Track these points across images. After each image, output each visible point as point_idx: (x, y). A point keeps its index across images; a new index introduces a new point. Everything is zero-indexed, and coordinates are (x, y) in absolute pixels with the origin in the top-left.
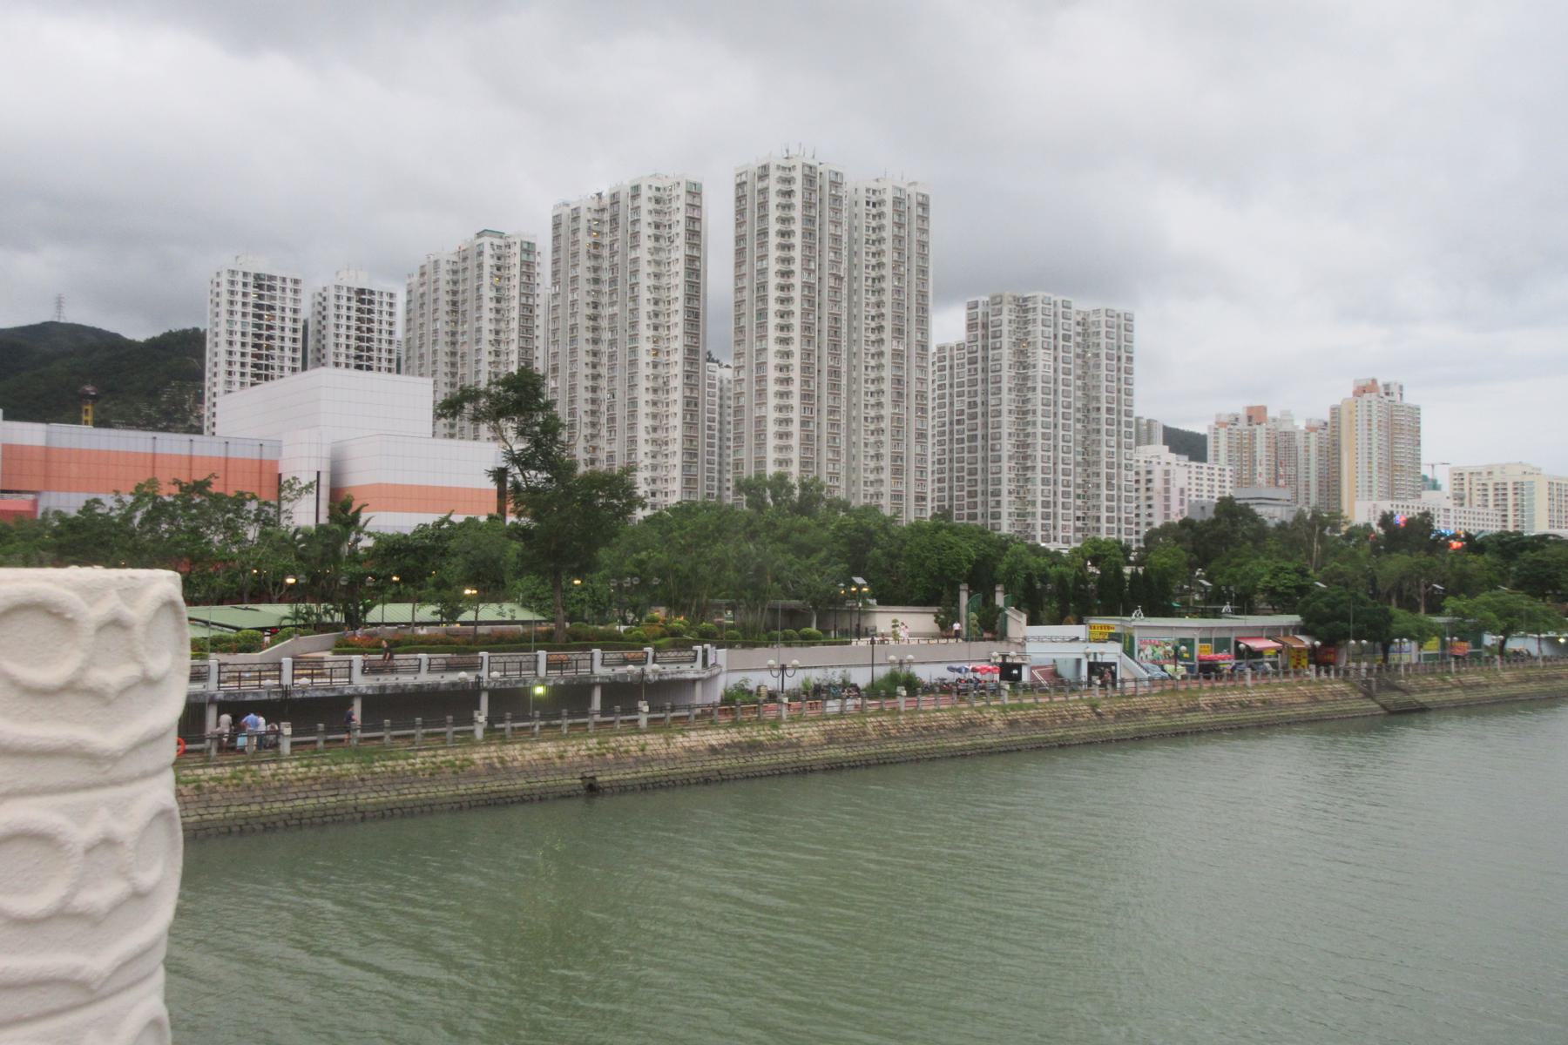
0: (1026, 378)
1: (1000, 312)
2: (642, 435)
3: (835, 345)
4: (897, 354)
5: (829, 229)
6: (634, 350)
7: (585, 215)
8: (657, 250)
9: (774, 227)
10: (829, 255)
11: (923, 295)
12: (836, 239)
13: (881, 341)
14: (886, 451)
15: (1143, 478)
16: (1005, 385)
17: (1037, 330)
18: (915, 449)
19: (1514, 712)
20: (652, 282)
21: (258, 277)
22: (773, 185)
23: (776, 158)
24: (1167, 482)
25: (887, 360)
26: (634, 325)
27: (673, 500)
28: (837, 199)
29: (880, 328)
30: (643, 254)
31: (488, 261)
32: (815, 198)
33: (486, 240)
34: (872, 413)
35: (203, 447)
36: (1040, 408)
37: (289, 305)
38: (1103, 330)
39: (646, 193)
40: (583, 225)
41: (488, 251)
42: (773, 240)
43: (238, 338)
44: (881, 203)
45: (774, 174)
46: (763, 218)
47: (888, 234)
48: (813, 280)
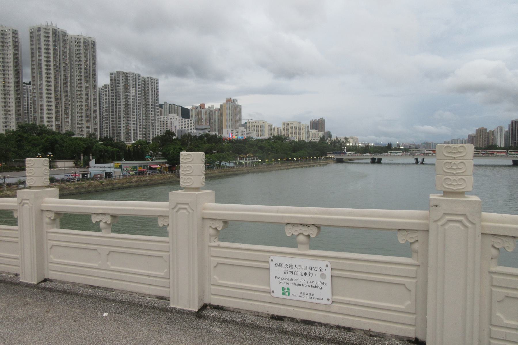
0: (128, 95)
1: (119, 77)
4: (86, 87)
10: (62, 57)
15: (165, 123)
16: (121, 97)
18: (93, 115)
24: (171, 124)
25: (83, 89)
28: (64, 40)
32: (57, 39)
34: (79, 104)
36: (132, 104)
45: (42, 31)
48: (58, 64)
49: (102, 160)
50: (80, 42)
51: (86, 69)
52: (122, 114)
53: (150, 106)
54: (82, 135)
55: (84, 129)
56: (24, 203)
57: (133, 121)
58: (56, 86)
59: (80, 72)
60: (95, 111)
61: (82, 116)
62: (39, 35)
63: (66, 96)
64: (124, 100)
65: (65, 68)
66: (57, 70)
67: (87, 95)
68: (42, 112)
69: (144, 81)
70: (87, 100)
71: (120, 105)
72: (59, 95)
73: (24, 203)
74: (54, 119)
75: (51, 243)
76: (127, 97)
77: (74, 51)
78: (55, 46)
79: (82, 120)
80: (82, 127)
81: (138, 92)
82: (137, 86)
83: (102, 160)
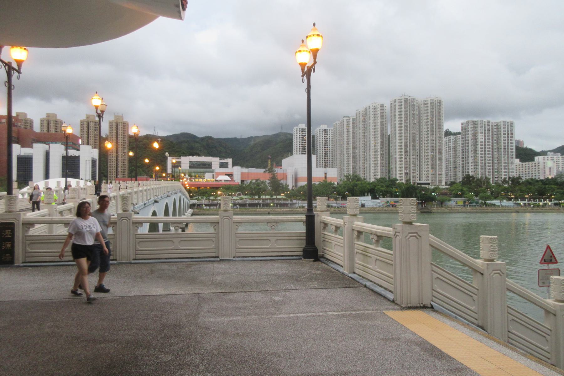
0: (476, 142)
2: (372, 162)
3: (414, 140)
4: (432, 140)
6: (370, 144)
7: (361, 113)
9: (397, 113)
10: (412, 118)
12: (414, 114)
13: (428, 137)
14: (430, 163)
15: (537, 165)
16: (470, 144)
17: (479, 129)
18: (438, 162)
20: (373, 127)
22: (397, 104)
23: (397, 98)
24: (544, 166)
25: (429, 142)
26: (370, 138)
27: (379, 177)
28: (414, 105)
29: (428, 134)
30: (371, 121)
31: (345, 123)
33: (345, 118)
34: (426, 154)
35: (205, 180)
36: (480, 150)
38: (502, 127)
39: (371, 107)
40: (361, 115)
41: (345, 121)
42: (397, 116)
43: (298, 143)
44: (428, 103)
45: (397, 101)
46: (395, 111)
47: (429, 111)
49: (21, 173)
50: (428, 103)
51: (432, 125)
52: (471, 160)
53: (503, 150)
54: (428, 180)
55: (430, 175)
56: (397, 236)
58: (406, 143)
59: (428, 128)
60: (440, 159)
61: (428, 165)
62: (395, 105)
63: (414, 149)
65: (414, 127)
66: (407, 130)
68: (396, 164)
71: (468, 152)
73: (397, 236)
74: (403, 169)
75: (356, 250)
76: (475, 144)
77: (423, 112)
78: (406, 111)
81: (487, 138)
82: (487, 132)
83: (21, 173)
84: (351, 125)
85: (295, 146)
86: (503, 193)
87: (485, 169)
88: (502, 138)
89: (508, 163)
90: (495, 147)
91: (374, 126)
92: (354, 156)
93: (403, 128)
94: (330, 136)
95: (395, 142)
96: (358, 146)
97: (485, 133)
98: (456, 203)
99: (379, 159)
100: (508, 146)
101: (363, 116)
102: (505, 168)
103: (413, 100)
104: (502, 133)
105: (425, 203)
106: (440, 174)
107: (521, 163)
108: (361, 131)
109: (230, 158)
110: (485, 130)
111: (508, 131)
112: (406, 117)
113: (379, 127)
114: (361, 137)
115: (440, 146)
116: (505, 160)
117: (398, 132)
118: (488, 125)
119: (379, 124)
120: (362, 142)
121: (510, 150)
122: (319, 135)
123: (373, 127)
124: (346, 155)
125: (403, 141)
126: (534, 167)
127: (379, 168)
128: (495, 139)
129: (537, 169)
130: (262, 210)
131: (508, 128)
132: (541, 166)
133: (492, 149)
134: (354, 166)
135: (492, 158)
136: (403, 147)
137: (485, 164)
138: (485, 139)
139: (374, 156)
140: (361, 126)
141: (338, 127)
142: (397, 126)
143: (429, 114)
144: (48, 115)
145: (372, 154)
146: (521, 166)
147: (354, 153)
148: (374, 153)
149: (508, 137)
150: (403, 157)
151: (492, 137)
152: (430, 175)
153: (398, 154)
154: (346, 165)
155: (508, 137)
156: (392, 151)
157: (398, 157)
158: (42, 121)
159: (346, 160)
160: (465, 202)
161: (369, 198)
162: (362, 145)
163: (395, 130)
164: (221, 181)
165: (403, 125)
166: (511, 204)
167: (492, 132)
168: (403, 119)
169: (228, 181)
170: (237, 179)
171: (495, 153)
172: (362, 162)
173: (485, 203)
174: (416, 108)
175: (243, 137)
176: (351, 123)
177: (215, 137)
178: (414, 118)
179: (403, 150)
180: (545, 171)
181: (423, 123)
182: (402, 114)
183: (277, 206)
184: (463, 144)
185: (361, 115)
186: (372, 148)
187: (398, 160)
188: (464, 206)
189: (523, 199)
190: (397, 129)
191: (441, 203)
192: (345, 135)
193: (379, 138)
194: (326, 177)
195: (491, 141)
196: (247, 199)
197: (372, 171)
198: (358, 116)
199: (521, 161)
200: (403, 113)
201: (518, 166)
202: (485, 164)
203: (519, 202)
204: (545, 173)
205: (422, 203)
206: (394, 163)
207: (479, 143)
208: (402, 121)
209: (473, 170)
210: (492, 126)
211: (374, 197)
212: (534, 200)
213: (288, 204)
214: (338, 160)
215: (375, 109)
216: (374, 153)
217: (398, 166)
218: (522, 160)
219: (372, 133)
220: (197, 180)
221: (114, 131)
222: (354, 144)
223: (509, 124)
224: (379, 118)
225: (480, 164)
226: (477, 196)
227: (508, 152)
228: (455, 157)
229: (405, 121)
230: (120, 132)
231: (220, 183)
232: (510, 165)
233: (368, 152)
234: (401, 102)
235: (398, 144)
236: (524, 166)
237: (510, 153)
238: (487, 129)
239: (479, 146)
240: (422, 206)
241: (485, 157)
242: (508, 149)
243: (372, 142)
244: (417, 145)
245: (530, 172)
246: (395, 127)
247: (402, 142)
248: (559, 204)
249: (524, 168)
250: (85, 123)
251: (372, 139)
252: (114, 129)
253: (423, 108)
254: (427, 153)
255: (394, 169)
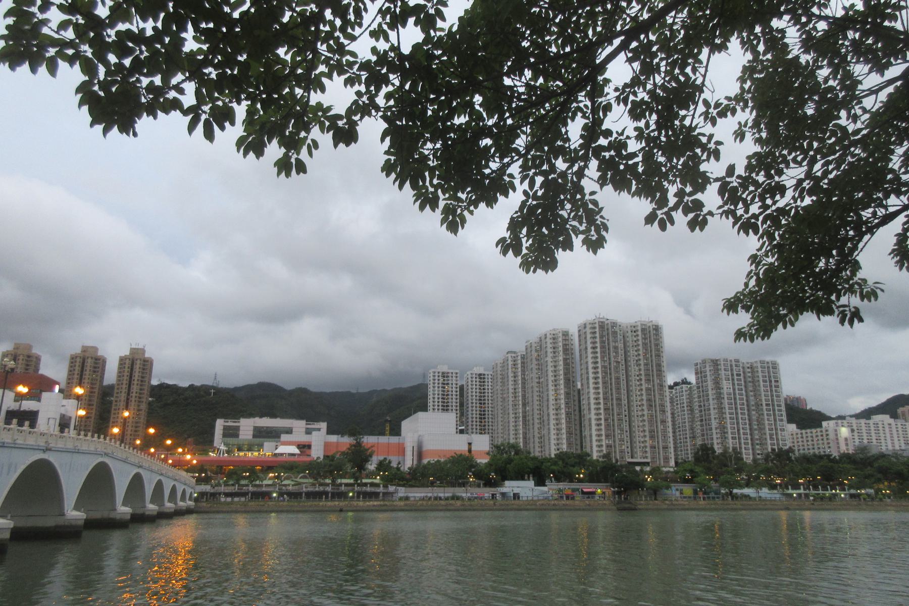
0: (720, 393)
1: (705, 367)
2: (552, 427)
3: (618, 389)
4: (648, 389)
5: (612, 344)
7: (534, 345)
8: (555, 357)
11: (659, 365)
12: (616, 348)
14: (647, 428)
15: (824, 434)
16: (711, 397)
18: (660, 427)
19: (186, 516)
20: (553, 369)
21: (443, 373)
22: (588, 331)
24: (837, 435)
25: (644, 392)
28: (615, 333)
30: (549, 359)
31: (510, 363)
32: (605, 333)
33: (509, 355)
34: (640, 413)
36: (727, 406)
37: (454, 382)
38: (760, 370)
40: (533, 348)
41: (510, 359)
43: (436, 396)
45: (588, 326)
47: (640, 343)
48: (607, 364)
51: (646, 364)
52: (714, 424)
53: (765, 407)
54: (646, 457)
57: (732, 433)
58: (605, 393)
59: (640, 370)
60: (663, 422)
63: (619, 405)
64: (715, 401)
65: (617, 368)
66: (606, 373)
67: (649, 400)
68: (590, 429)
69: (751, 367)
70: (650, 406)
71: (709, 410)
72: (609, 404)
74: (603, 437)
76: (719, 397)
77: (630, 344)
78: (602, 342)
79: (645, 436)
80: (646, 447)
81: (737, 387)
82: (736, 377)
84: (519, 366)
85: (431, 400)
86: (763, 477)
87: (739, 438)
88: (762, 388)
89: (776, 429)
90: (753, 403)
91: (554, 365)
92: (524, 417)
93: (599, 370)
94: (489, 384)
95: (589, 392)
96: (530, 399)
97: (733, 380)
98: (681, 493)
99: (564, 421)
100: (772, 400)
101: (536, 351)
102: (771, 439)
103: (614, 324)
104: (761, 379)
105: (625, 491)
106: (666, 448)
107: (799, 431)
108: (534, 375)
109: (323, 421)
110: (732, 375)
111: (770, 377)
112: (603, 352)
113: (561, 367)
114: (535, 384)
115: (661, 400)
116: (770, 425)
117: (591, 375)
118: (736, 366)
119: (561, 363)
120: (536, 394)
121: (776, 408)
122: (470, 383)
123: (553, 369)
124: (512, 416)
125: (601, 391)
126: (820, 438)
127: (564, 436)
128: (751, 389)
129: (825, 442)
130: (329, 503)
131: (769, 372)
132: (832, 436)
133: (748, 406)
134: (525, 434)
135: (749, 420)
136: (601, 401)
137: (738, 430)
138: (734, 390)
139: (554, 417)
140: (534, 366)
141: (499, 369)
142: (591, 366)
143: (640, 347)
144: (134, 351)
145: (552, 412)
146: (799, 436)
147: (524, 412)
148: (554, 412)
149: (771, 386)
150: (602, 417)
151: (745, 387)
152: (648, 449)
153: (593, 412)
154: (512, 432)
155: (771, 386)
156: (585, 407)
157: (593, 417)
158: (122, 360)
159: (512, 424)
160: (695, 492)
161: (531, 483)
162: (536, 398)
163: (587, 373)
164: (282, 454)
165: (599, 365)
166: (775, 495)
167: (745, 377)
168: (599, 355)
169: (293, 455)
170: (317, 453)
171: (754, 413)
172: (537, 426)
173: (731, 492)
174: (619, 337)
175: (361, 391)
176: (519, 362)
177: (312, 389)
178: (617, 353)
179: (602, 406)
180: (838, 443)
181: (632, 363)
182: (596, 347)
183: (358, 497)
184: (699, 397)
185: (533, 348)
186: (552, 402)
187: (594, 422)
188: (695, 498)
189: (796, 486)
190: (591, 371)
191: (655, 492)
192: (511, 383)
193: (562, 387)
194: (470, 451)
195: (744, 392)
196: (306, 484)
197: (553, 442)
198: (529, 350)
199: (798, 428)
200: (598, 345)
201: (795, 436)
202: (738, 430)
203: (790, 491)
204: (839, 447)
205: (619, 493)
206: (587, 428)
207: (726, 396)
208: (597, 357)
209: (719, 441)
210: (743, 368)
211: (540, 482)
212: (816, 488)
213: (379, 493)
214: (500, 423)
215: (554, 339)
216: (554, 412)
217: (594, 433)
218: (801, 426)
219: (551, 378)
220: (242, 454)
221: (126, 374)
222: (524, 396)
223: (771, 365)
224: (561, 353)
225: (730, 431)
226: (716, 481)
227: (774, 410)
228: (692, 421)
229: (602, 357)
230: (136, 375)
231: (280, 458)
232: (779, 432)
233: (545, 409)
234: (595, 328)
235: (592, 396)
236: (804, 436)
237: (777, 413)
238: (735, 373)
239: (726, 401)
240: (620, 497)
241: (737, 419)
242: (773, 405)
243: (551, 393)
244: (624, 397)
245: (816, 447)
246: (587, 368)
247: (599, 393)
248: (859, 495)
249: (805, 439)
250: (78, 360)
251: (551, 388)
252: (126, 370)
253: (630, 339)
254: (641, 412)
255: (588, 439)
